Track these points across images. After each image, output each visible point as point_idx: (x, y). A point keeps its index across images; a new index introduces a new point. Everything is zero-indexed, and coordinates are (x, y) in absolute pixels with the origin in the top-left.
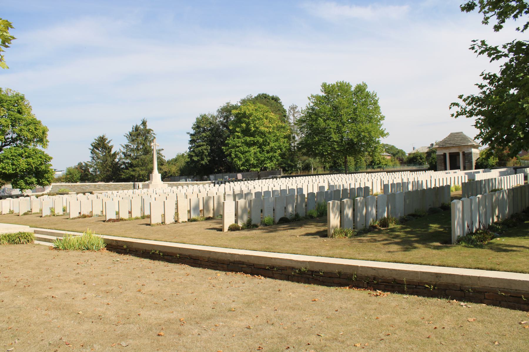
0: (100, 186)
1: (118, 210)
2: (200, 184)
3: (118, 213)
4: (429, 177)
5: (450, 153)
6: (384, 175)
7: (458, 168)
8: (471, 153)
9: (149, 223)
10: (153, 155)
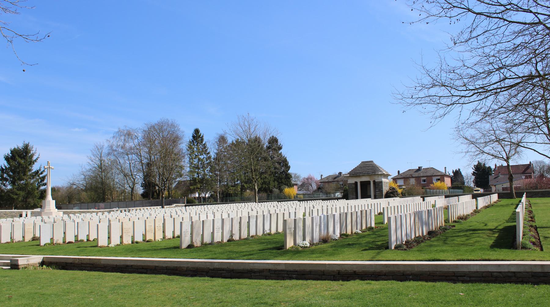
1: (76, 234)
2: (93, 212)
3: (76, 236)
4: (321, 207)
5: (361, 182)
7: (369, 197)
8: (381, 182)
9: (38, 244)
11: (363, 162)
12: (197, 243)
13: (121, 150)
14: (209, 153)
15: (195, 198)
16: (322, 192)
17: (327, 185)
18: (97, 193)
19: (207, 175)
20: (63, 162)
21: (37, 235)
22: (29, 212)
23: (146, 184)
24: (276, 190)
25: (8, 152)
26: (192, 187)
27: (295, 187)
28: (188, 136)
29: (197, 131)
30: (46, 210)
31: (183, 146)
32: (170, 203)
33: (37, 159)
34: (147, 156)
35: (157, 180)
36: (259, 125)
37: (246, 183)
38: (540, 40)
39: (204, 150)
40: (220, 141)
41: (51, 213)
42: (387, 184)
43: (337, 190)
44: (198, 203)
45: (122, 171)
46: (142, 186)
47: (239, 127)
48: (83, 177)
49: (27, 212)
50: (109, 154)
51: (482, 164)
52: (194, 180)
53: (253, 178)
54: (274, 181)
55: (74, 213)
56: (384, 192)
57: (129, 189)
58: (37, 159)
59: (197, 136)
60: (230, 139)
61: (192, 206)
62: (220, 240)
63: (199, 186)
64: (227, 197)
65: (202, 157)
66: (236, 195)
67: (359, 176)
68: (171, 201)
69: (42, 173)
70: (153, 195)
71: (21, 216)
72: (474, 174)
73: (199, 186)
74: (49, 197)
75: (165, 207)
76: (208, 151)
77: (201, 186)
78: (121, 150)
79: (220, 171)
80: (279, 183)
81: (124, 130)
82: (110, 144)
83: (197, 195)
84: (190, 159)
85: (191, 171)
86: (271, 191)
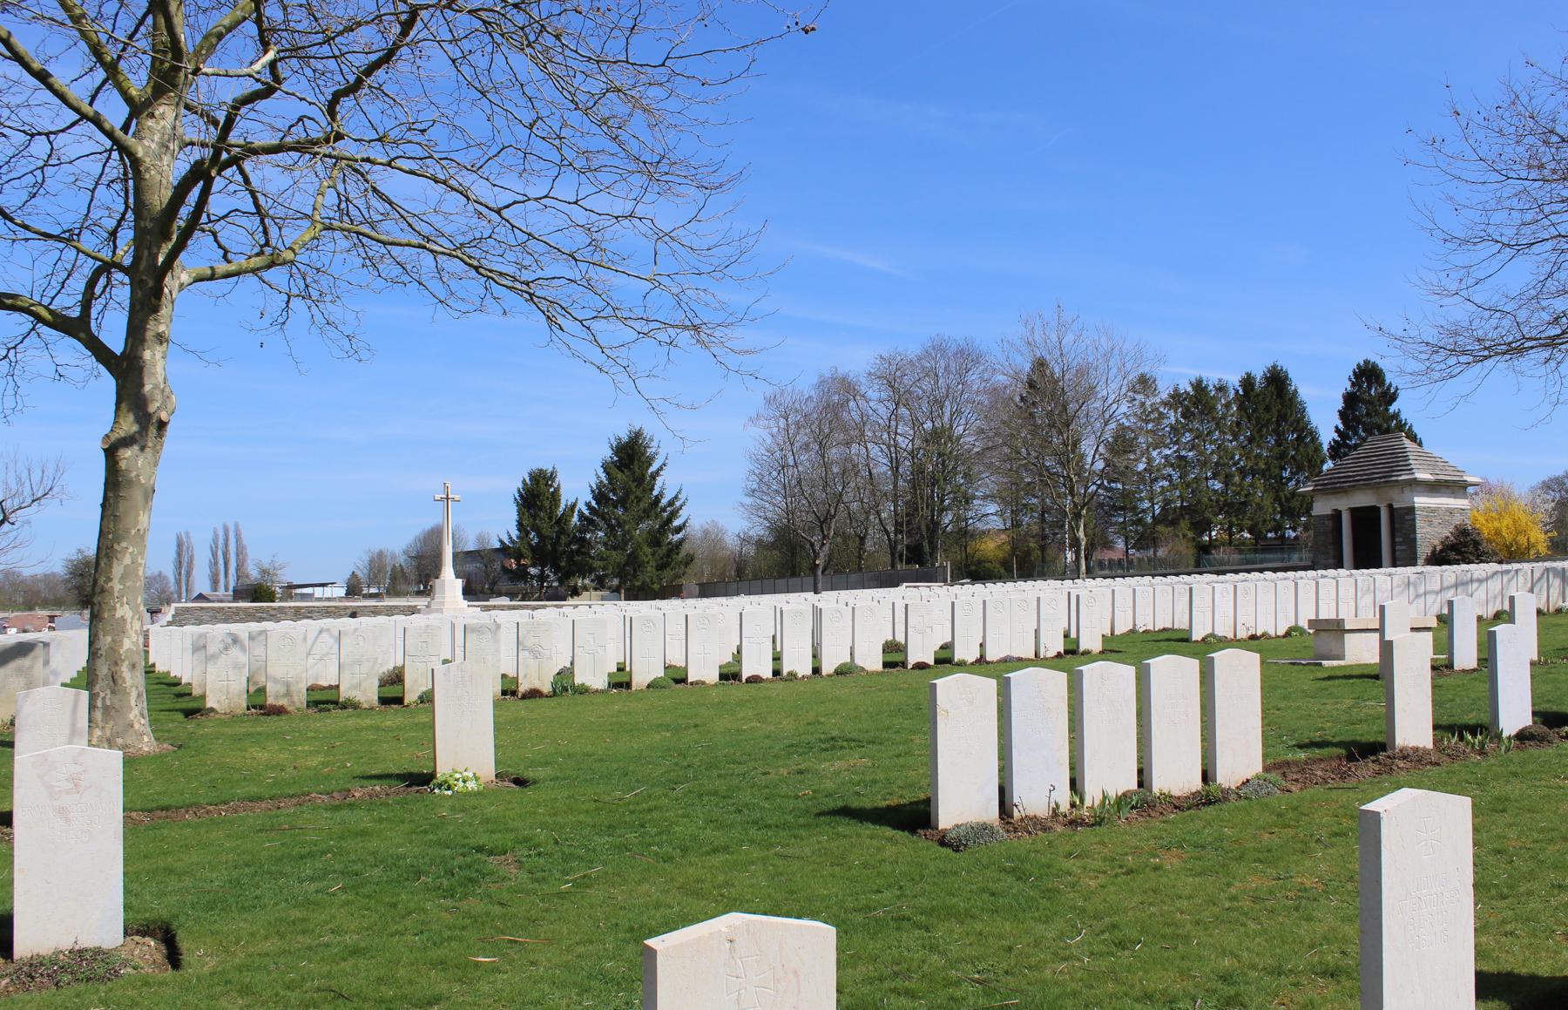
18: (791, 557)
21: (900, 638)
29: (1368, 374)
33: (661, 469)
38: (30, 179)
49: (817, 613)
56: (1423, 550)
58: (661, 469)
74: (448, 571)
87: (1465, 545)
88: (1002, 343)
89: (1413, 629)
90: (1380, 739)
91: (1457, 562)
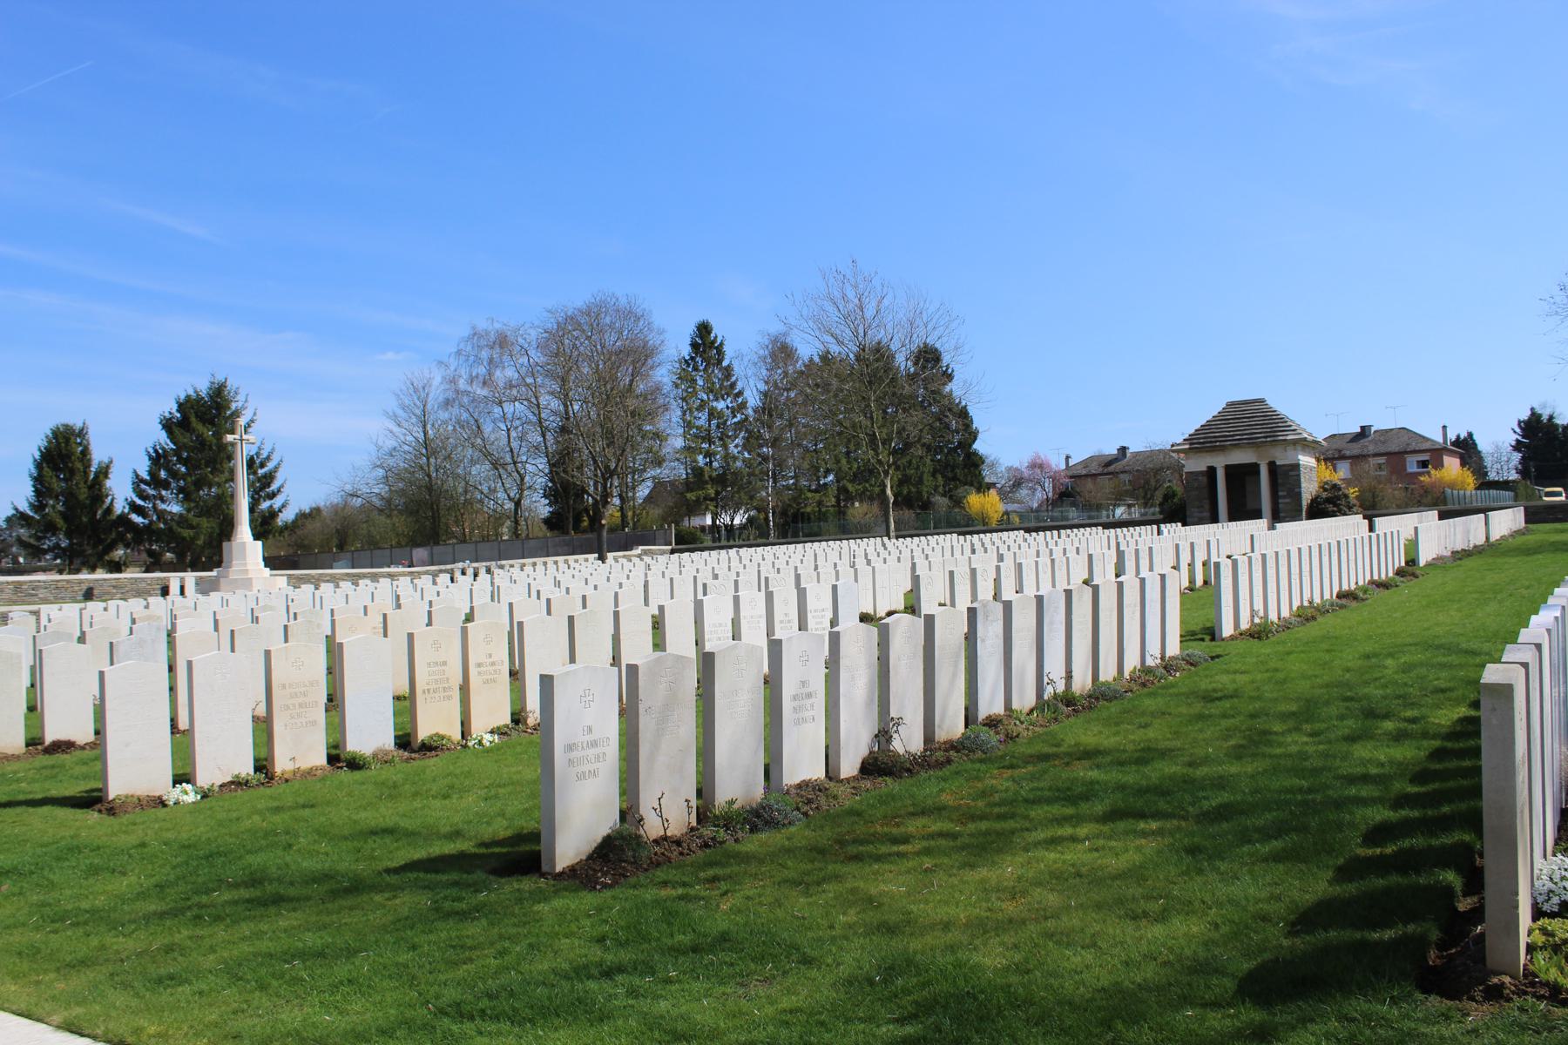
0: (35, 586)
5: (1228, 468)
6: (1020, 540)
7: (1256, 514)
8: (1296, 467)
10: (232, 472)
11: (1231, 404)
12: (668, 808)
13: (481, 392)
14: (740, 393)
15: (703, 529)
16: (1074, 504)
17: (1089, 484)
18: (419, 520)
19: (735, 458)
20: (321, 437)
22: (190, 577)
23: (556, 490)
24: (941, 501)
25: (170, 407)
26: (691, 496)
27: (993, 492)
28: (678, 345)
29: (704, 329)
30: (235, 570)
31: (663, 375)
32: (626, 546)
34: (555, 404)
35: (588, 479)
36: (890, 296)
37: (855, 478)
39: (727, 386)
40: (773, 355)
41: (247, 583)
42: (1312, 476)
43: (1118, 499)
44: (710, 544)
45: (487, 454)
46: (545, 496)
47: (831, 309)
48: (381, 472)
49: (182, 579)
50: (447, 403)
51: (1545, 418)
52: (698, 472)
53: (880, 462)
54: (933, 475)
55: (335, 580)
56: (1306, 499)
57: (509, 506)
59: (705, 343)
60: (807, 349)
61: (692, 550)
62: (815, 771)
63: (712, 492)
64: (795, 523)
65: (720, 405)
66: (822, 517)
67: (1222, 449)
68: (629, 536)
69: (262, 465)
70: (578, 521)
71: (165, 592)
72: (1518, 447)
73: (712, 492)
74: (244, 531)
75: (610, 555)
76: (739, 386)
77: (717, 493)
78: (481, 392)
79: (775, 443)
80: (948, 480)
81: (487, 333)
82: (450, 372)
83: (709, 521)
84: (684, 413)
85: (687, 449)
86: (926, 506)
87: (1338, 498)
88: (531, 305)
89: (385, 635)
90: (529, 825)
91: (1333, 515)
